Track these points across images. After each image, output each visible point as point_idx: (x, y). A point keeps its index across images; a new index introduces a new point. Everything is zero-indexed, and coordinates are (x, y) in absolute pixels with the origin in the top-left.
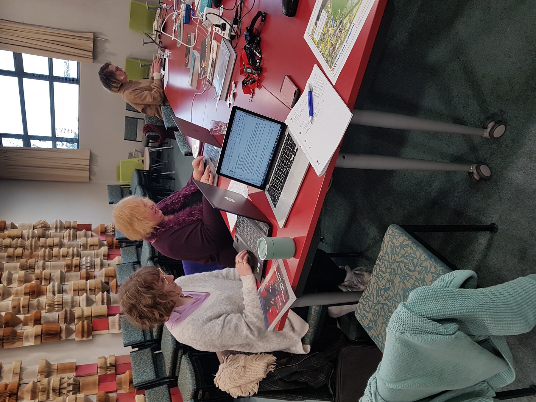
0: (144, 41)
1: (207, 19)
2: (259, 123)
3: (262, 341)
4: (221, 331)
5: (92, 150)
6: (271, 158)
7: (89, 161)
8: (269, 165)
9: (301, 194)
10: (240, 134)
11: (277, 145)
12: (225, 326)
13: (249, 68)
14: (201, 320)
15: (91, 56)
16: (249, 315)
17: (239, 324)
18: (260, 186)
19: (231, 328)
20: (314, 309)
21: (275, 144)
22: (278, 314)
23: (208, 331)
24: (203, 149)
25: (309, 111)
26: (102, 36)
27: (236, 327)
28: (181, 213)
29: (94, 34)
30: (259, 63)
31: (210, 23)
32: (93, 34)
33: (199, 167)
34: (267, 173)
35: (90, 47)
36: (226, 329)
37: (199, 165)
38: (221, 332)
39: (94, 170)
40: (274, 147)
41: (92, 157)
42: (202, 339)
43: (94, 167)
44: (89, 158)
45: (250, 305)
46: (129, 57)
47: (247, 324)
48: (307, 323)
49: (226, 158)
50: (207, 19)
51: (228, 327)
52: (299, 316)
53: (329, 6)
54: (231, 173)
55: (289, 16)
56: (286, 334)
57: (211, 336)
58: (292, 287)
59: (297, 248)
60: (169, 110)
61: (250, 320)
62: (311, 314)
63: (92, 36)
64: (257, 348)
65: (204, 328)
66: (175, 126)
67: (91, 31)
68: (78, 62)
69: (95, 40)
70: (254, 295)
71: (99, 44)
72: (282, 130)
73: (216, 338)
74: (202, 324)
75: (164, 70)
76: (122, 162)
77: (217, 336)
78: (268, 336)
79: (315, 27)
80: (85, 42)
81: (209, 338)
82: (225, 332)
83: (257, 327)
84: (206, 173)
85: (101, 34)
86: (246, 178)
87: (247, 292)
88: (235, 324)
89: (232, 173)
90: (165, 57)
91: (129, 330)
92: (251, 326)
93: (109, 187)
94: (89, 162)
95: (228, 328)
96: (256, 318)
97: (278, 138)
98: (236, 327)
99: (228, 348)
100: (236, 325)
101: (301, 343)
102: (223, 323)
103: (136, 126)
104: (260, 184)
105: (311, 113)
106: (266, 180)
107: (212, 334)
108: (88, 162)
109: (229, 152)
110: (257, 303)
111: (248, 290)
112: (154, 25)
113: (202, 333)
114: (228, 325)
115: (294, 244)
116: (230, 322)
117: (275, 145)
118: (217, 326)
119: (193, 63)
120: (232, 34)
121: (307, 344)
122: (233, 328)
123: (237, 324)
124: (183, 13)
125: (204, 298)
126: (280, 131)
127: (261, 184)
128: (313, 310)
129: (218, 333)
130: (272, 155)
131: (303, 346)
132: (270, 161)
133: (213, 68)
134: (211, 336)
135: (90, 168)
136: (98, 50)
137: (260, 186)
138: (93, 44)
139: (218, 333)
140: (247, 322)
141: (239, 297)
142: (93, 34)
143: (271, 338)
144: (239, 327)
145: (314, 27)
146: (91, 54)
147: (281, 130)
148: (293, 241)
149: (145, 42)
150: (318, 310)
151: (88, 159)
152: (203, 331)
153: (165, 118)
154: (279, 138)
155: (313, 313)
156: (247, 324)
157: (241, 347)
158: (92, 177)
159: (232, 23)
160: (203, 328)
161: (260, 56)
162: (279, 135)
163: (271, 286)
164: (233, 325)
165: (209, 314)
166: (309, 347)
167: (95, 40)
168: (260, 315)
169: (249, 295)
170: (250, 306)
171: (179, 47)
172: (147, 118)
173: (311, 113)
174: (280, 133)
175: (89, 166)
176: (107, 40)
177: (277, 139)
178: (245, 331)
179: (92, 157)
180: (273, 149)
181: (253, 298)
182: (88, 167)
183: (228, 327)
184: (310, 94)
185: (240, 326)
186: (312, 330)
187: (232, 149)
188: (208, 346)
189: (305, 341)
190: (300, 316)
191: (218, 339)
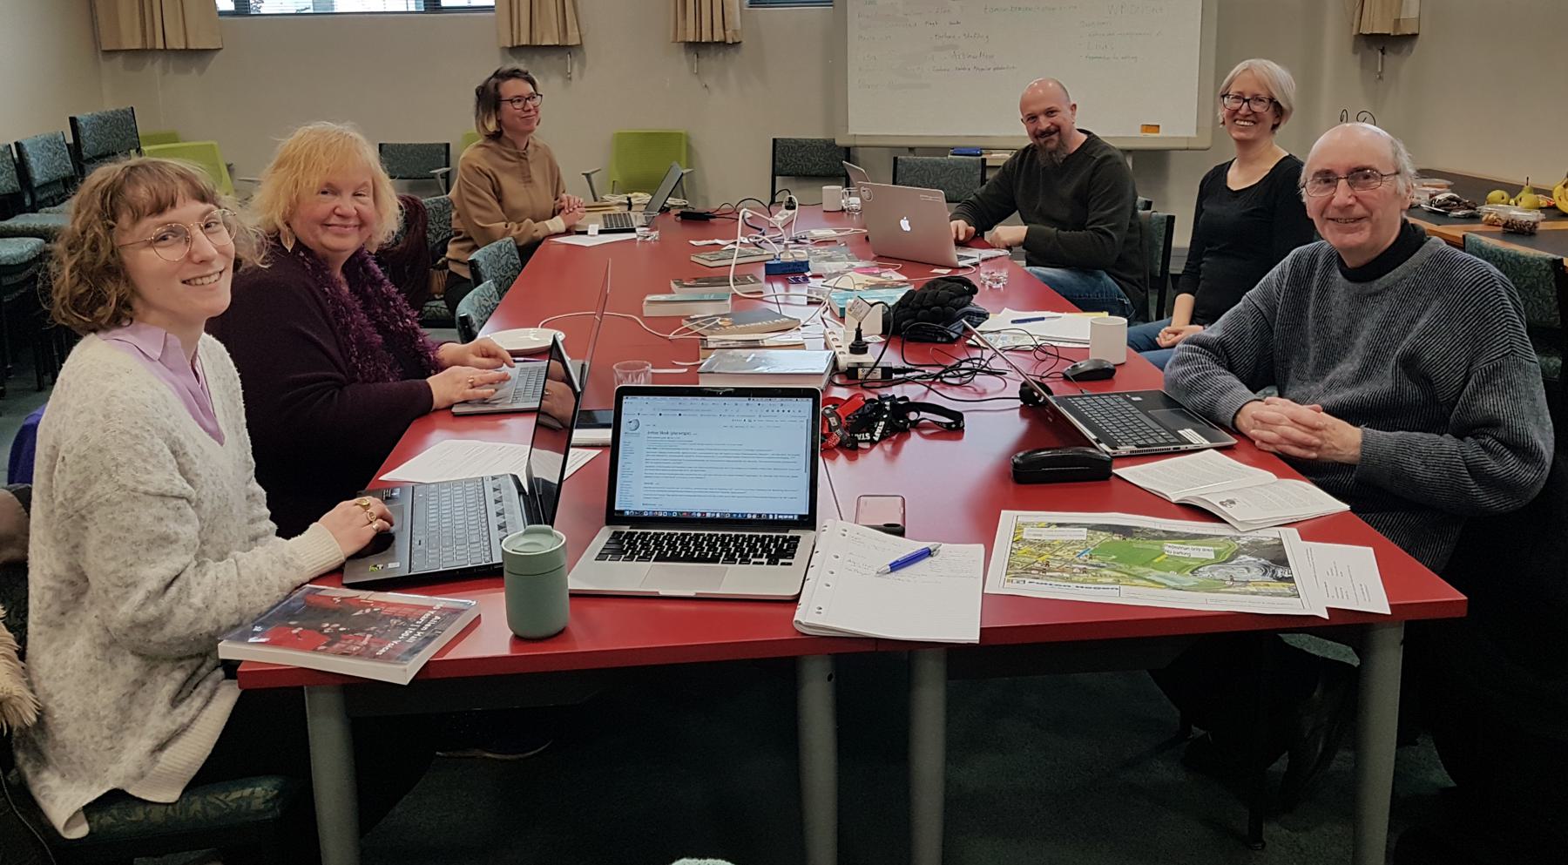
0: (593, 173)
1: (872, 305)
2: (793, 460)
3: (89, 651)
4: (152, 490)
5: (218, 55)
6: (708, 515)
7: (183, 47)
8: (689, 516)
9: (692, 607)
10: (750, 421)
11: (751, 521)
12: (167, 500)
13: (839, 419)
14: (170, 423)
15: (519, 40)
16: (208, 577)
17: (174, 546)
18: (616, 508)
19: (164, 523)
20: (253, 793)
21: (752, 514)
22: (315, 650)
23: (145, 450)
24: (522, 359)
25: (897, 561)
26: (576, 66)
27: (166, 540)
28: (363, 318)
29: (580, 46)
30: (863, 438)
31: (862, 314)
32: (579, 43)
33: (477, 356)
34: (662, 518)
35: (542, 38)
36: (158, 508)
37: (483, 356)
38: (146, 493)
39: (149, 64)
40: (742, 514)
41: (194, 56)
42: (115, 437)
43: (159, 62)
44: (192, 46)
45: (242, 572)
46: (688, 137)
47: (177, 577)
48: (184, 791)
49: (671, 402)
50: (872, 305)
51: (163, 512)
52: (209, 752)
53: (1102, 538)
54: (633, 425)
55: (1014, 471)
56: (128, 728)
57: (130, 461)
58: (428, 662)
59: (555, 639)
60: (508, 258)
61: (193, 584)
62: (228, 791)
63: (573, 40)
64: (54, 645)
65: (153, 437)
66: (484, 279)
67: (583, 39)
68: (492, 7)
69: (562, 49)
70: (281, 578)
71: (554, 59)
72: (796, 521)
73: (122, 481)
74: (162, 429)
75: (601, 232)
76: (212, 145)
77: (131, 484)
78: (114, 667)
79: (1043, 525)
80: (555, 25)
81: (121, 459)
82: (149, 506)
83: (171, 612)
84: (490, 374)
85: (583, 63)
86: (627, 466)
87: (283, 555)
88: (176, 533)
89: (633, 428)
90: (637, 230)
91: (830, 162)
92: (174, 589)
93: (127, 113)
94: (177, 47)
95: (162, 515)
96: (204, 600)
97: (771, 517)
98: (166, 540)
99: (471, 475)
100: (174, 537)
101: (91, 798)
102: (176, 493)
103: (405, 176)
104: (622, 509)
105: (896, 566)
106: (639, 520)
107: (139, 463)
108: (176, 42)
109: (691, 407)
110: (254, 593)
111: (293, 556)
112: (640, 194)
113: (137, 432)
114: (171, 513)
115: (554, 632)
116: (180, 517)
117: (749, 517)
118: (168, 477)
119: (706, 298)
120: (860, 370)
121: (89, 822)
122: (161, 529)
123: (176, 541)
124: (788, 257)
125: (210, 425)
126: (791, 517)
127: (622, 512)
128: (247, 792)
129: (142, 483)
130: (718, 516)
131: (77, 812)
132: (699, 515)
133: (740, 344)
134: (130, 461)
135: (154, 50)
136: (537, 58)
137: (616, 508)
138: (552, 44)
139: (142, 483)
140: (182, 576)
141: (231, 539)
142: (579, 43)
143: (106, 680)
144: (166, 551)
145: (1040, 523)
146: (525, 41)
147: (796, 518)
148: (560, 627)
149: (593, 176)
150: (253, 808)
151: (186, 43)
152: (146, 435)
153: (489, 251)
154: (773, 520)
155: (236, 795)
156: (177, 577)
157: (58, 586)
158: (120, 59)
159: (885, 365)
160: (153, 432)
161: (876, 439)
162: (780, 517)
163: (372, 611)
164: (171, 527)
165: (190, 449)
166: (81, 831)
167: (562, 49)
168: (214, 614)
169: (273, 562)
170: (239, 574)
171: (693, 259)
172: (437, 205)
173: (896, 566)
174: (786, 517)
175: (162, 47)
176: (570, 79)
177: (768, 515)
178: (153, 573)
179: (194, 56)
180: (738, 514)
181: (269, 575)
182: (160, 45)
183: (163, 512)
184: (928, 553)
185: (168, 554)
186: (157, 816)
187: (703, 413)
188: (85, 463)
189: (98, 811)
190: (210, 756)
191: (121, 487)
